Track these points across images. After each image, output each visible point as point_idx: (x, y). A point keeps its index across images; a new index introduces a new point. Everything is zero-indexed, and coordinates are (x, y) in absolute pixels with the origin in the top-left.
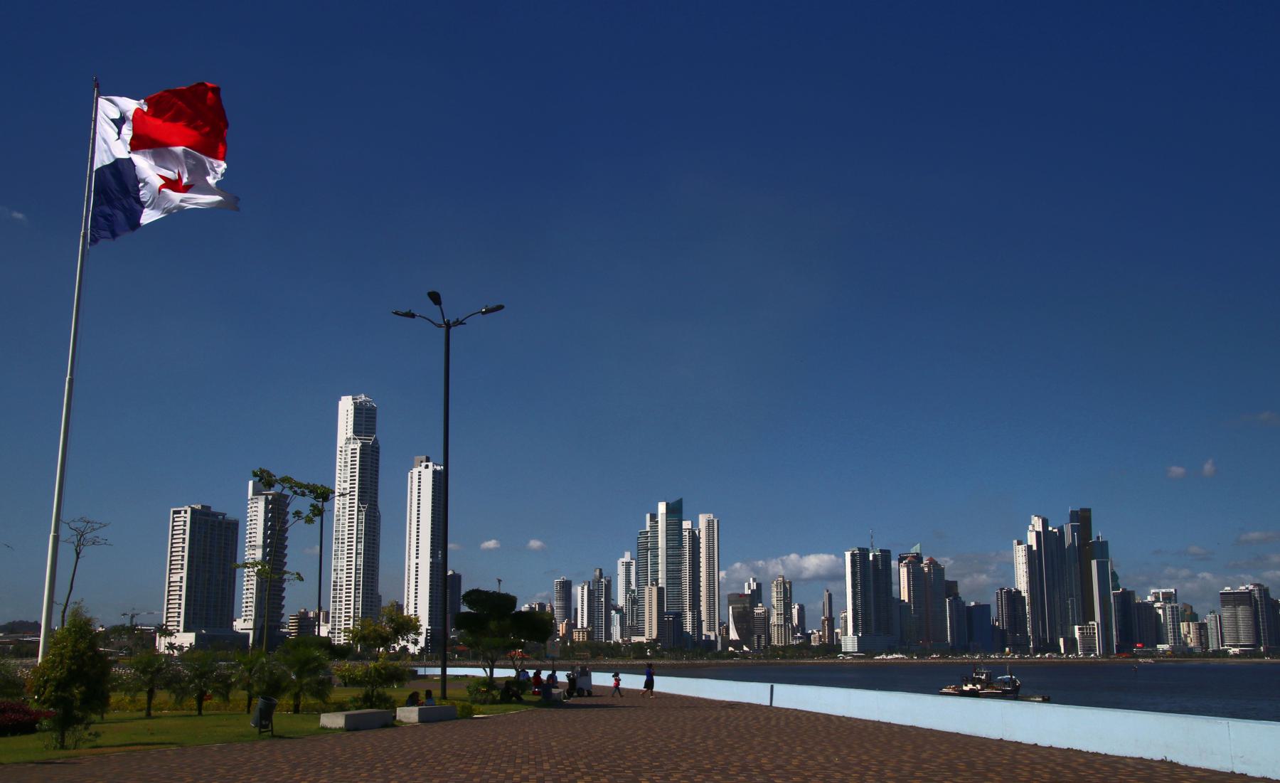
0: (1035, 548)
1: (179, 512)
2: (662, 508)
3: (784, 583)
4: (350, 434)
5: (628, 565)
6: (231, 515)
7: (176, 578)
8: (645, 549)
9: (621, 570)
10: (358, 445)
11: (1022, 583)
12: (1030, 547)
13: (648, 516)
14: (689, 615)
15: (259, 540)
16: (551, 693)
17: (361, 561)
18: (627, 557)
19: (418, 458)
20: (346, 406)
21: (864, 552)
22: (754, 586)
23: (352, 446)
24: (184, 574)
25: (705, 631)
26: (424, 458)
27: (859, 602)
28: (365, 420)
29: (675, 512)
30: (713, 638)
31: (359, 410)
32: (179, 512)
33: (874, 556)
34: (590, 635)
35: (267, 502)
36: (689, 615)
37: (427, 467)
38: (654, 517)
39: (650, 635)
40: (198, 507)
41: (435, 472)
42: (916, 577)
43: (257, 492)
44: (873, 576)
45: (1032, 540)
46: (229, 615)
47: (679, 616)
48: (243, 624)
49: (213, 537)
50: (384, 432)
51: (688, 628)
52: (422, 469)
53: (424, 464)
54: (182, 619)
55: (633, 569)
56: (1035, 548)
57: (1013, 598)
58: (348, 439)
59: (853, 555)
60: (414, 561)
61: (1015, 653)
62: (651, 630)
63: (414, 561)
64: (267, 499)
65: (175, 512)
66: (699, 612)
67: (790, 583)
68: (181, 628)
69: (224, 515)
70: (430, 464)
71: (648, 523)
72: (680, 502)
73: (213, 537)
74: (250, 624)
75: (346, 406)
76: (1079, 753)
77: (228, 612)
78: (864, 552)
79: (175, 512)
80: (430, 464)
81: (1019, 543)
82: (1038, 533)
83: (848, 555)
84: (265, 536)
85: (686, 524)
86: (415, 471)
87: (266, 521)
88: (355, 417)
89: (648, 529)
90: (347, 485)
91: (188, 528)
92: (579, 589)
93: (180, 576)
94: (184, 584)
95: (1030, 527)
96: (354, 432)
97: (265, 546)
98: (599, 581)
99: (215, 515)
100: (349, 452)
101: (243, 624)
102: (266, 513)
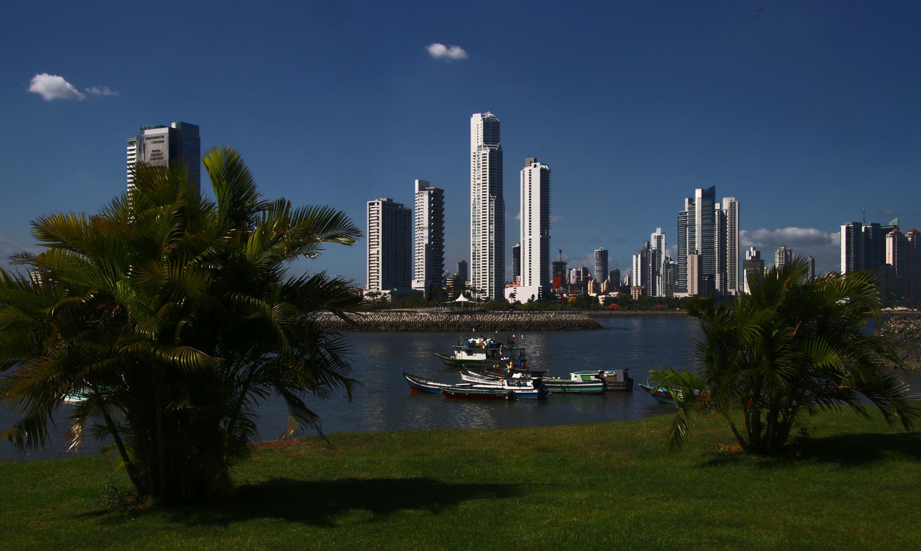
1: (373, 204)
2: (698, 193)
3: (786, 251)
4: (481, 143)
5: (659, 239)
6: (407, 206)
7: (374, 251)
8: (685, 224)
10: (487, 151)
13: (687, 200)
14: (718, 276)
15: (426, 223)
16: (38, 96)
17: (493, 238)
18: (658, 232)
19: (528, 160)
20: (477, 122)
21: (857, 226)
22: (754, 253)
23: (483, 152)
24: (380, 249)
25: (729, 290)
26: (533, 159)
27: (852, 266)
28: (491, 132)
29: (709, 197)
30: (733, 294)
32: (373, 204)
33: (866, 229)
34: (644, 292)
35: (430, 196)
36: (718, 276)
37: (535, 166)
38: (692, 201)
39: (692, 291)
40: (385, 199)
41: (542, 170)
43: (422, 188)
44: (865, 245)
47: (712, 277)
48: (418, 284)
49: (397, 221)
50: (505, 141)
51: (717, 287)
52: (532, 168)
53: (533, 164)
54: (380, 281)
55: (663, 241)
58: (479, 147)
59: (848, 228)
60: (527, 237)
62: (692, 288)
63: (527, 237)
64: (429, 193)
65: (370, 204)
66: (726, 274)
67: (791, 251)
69: (402, 205)
70: (538, 164)
71: (687, 206)
72: (714, 187)
73: (397, 221)
74: (422, 284)
75: (477, 122)
76: (199, 144)
77: (408, 276)
78: (857, 226)
79: (370, 204)
80: (538, 164)
83: (843, 228)
84: (430, 221)
85: (717, 206)
86: (527, 169)
87: (430, 209)
88: (484, 129)
89: (687, 210)
90: (480, 181)
91: (380, 215)
92: (634, 257)
93: (377, 250)
94: (380, 256)
96: (484, 141)
97: (430, 228)
98: (647, 251)
99: (397, 205)
100: (481, 156)
101: (418, 284)
102: (430, 203)
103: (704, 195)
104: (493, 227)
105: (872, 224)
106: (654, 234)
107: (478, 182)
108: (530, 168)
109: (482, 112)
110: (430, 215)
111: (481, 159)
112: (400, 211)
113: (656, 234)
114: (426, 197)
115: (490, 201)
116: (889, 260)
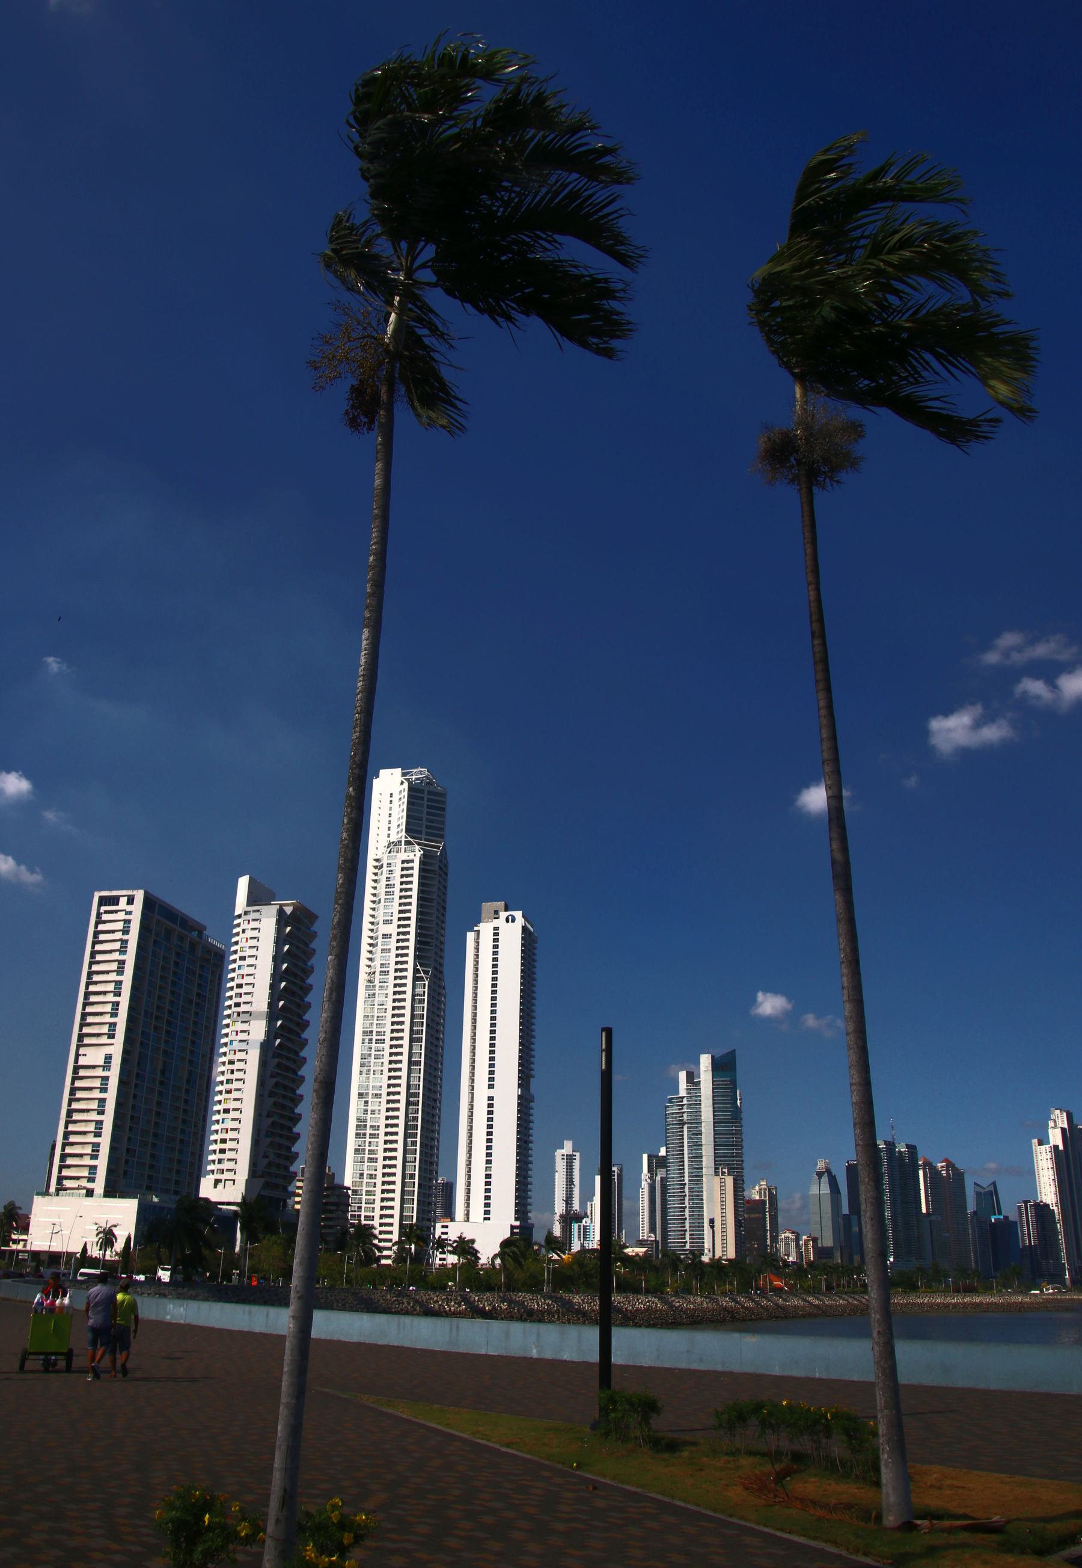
0: (1061, 1148)
1: (115, 901)
4: (398, 832)
5: (570, 1159)
7: (93, 1056)
9: (560, 1166)
10: (416, 854)
11: (1048, 1193)
12: (1056, 1147)
13: (682, 1076)
15: (260, 999)
18: (568, 1148)
19: (487, 907)
23: (404, 856)
28: (424, 815)
31: (416, 795)
35: (282, 919)
38: (691, 1078)
42: (934, 1177)
43: (256, 898)
45: (1056, 1138)
46: (193, 1165)
48: (225, 1183)
52: (500, 922)
53: (503, 915)
54: (102, 1163)
55: (577, 1164)
56: (1061, 1148)
57: (1042, 1209)
61: (625, 1268)
64: (281, 912)
65: (103, 901)
68: (99, 1186)
73: (180, 975)
79: (103, 901)
81: (1040, 1143)
82: (1063, 1130)
84: (275, 994)
86: (486, 929)
87: (277, 959)
89: (683, 1092)
90: (392, 929)
94: (114, 1075)
95: (1051, 1124)
97: (272, 1014)
101: (225, 1183)
102: (279, 942)
103: (717, 1067)
104: (421, 1049)
105: (907, 1146)
106: (559, 1153)
107: (383, 929)
108: (496, 923)
109: (404, 764)
110: (277, 976)
111: (398, 873)
112: (193, 946)
113: (564, 1152)
114: (267, 923)
115: (416, 979)
116: (924, 1211)
